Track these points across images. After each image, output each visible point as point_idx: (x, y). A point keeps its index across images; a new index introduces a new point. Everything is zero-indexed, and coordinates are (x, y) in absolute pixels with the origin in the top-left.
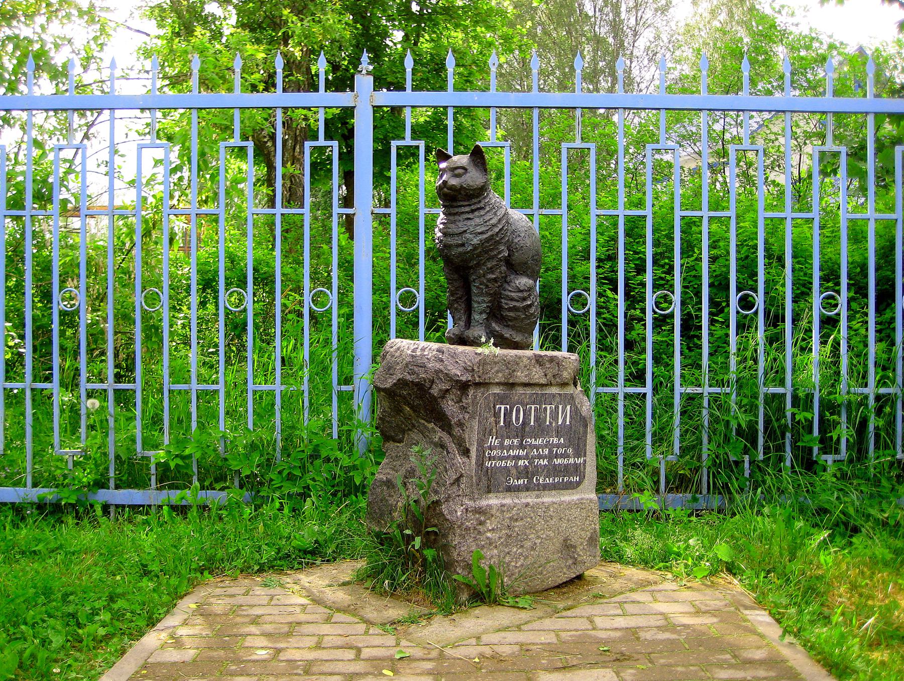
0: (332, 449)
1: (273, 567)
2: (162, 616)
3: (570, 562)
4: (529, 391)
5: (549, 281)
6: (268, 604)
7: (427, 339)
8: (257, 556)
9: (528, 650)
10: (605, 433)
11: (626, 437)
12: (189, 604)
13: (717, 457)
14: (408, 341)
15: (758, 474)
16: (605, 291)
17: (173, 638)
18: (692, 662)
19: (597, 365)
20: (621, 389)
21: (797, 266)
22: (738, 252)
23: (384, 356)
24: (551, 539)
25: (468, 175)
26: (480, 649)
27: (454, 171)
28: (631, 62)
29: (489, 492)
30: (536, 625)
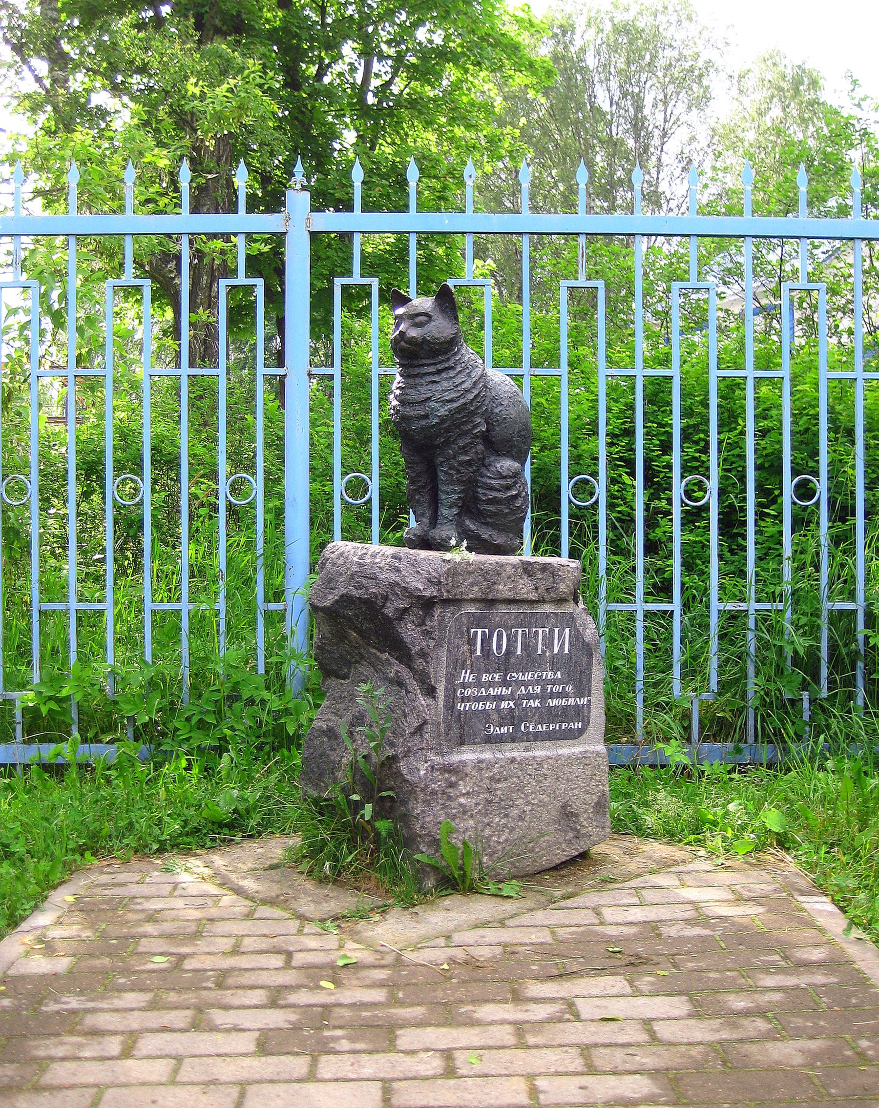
0: (257, 688)
1: (177, 845)
2: (27, 913)
3: (571, 835)
4: (514, 610)
5: (545, 463)
6: (171, 895)
7: (383, 541)
8: (156, 831)
9: (513, 953)
10: (618, 663)
11: (647, 669)
12: (64, 896)
13: (767, 694)
14: (356, 544)
15: (821, 716)
16: (620, 476)
17: (41, 941)
18: (730, 965)
19: (608, 575)
20: (640, 606)
21: (872, 442)
22: (794, 423)
23: (323, 564)
24: (544, 805)
25: (433, 323)
26: (450, 952)
27: (417, 318)
28: (658, 172)
29: (462, 743)
30: (525, 919)
